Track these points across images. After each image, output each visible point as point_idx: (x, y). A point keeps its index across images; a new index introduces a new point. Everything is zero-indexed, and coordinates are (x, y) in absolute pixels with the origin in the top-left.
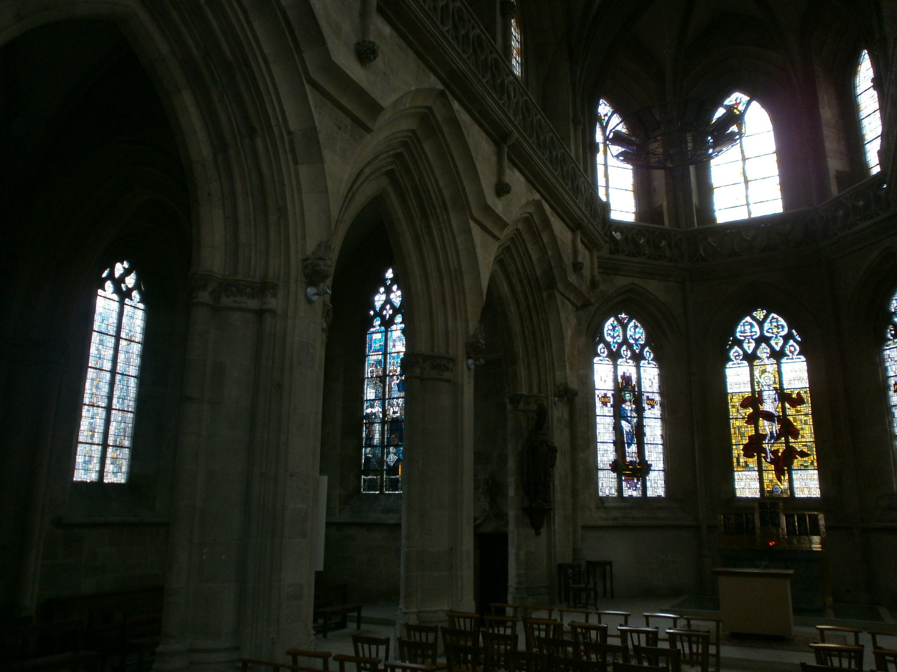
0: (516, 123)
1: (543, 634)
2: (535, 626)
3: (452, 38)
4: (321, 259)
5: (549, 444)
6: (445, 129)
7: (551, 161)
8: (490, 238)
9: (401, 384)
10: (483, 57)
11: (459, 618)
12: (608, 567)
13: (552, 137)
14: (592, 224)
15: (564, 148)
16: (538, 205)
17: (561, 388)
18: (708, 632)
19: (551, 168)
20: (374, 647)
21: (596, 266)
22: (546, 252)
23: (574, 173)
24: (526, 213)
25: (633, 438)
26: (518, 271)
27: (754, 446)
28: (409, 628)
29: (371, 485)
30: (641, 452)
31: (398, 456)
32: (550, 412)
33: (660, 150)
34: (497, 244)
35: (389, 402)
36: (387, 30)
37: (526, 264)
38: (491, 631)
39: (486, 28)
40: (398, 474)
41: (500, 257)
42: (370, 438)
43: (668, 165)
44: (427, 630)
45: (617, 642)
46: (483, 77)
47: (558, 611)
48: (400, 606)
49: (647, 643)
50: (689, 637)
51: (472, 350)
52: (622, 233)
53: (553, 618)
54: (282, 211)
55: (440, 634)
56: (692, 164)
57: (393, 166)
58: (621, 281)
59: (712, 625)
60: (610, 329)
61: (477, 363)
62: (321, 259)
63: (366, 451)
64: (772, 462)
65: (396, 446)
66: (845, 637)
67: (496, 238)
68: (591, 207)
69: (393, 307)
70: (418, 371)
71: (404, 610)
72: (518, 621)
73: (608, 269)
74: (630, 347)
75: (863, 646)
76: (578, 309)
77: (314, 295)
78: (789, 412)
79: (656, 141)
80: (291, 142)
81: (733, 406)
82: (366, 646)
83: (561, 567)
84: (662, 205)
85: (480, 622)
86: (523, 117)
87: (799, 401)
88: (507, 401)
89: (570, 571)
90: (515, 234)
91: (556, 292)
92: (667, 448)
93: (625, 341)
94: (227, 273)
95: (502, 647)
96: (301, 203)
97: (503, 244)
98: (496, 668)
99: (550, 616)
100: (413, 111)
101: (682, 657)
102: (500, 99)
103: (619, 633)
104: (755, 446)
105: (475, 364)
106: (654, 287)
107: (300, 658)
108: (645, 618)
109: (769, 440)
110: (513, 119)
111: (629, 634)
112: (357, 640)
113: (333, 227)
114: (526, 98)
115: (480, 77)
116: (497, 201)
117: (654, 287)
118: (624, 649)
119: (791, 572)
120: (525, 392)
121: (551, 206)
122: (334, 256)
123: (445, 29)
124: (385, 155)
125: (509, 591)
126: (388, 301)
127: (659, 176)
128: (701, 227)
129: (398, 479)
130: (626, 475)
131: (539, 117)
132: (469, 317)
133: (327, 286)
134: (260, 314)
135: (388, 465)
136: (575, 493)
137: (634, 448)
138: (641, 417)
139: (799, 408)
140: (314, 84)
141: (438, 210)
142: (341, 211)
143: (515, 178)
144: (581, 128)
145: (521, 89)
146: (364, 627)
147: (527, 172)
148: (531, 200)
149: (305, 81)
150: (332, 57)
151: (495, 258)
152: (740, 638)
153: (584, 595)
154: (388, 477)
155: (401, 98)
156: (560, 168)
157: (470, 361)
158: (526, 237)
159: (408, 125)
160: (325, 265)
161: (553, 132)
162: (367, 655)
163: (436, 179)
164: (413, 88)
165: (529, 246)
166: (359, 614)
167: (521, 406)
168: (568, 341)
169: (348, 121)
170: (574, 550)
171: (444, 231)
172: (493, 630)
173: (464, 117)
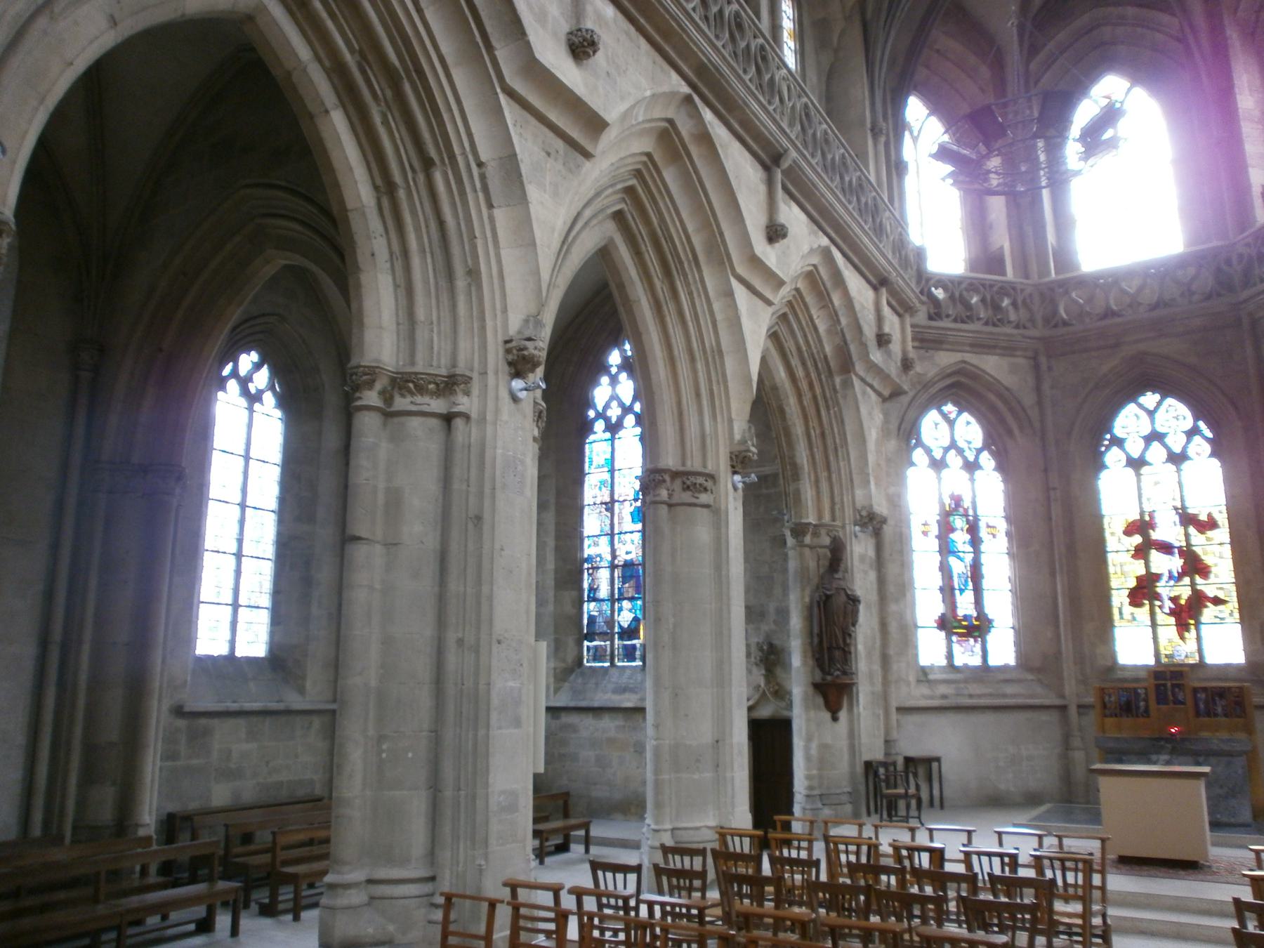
0: (793, 137)
1: (853, 858)
2: (842, 847)
3: (700, 19)
4: (529, 339)
5: (849, 593)
6: (694, 150)
7: (843, 190)
9: (636, 513)
10: (743, 45)
11: (732, 835)
12: (935, 765)
13: (843, 155)
14: (903, 279)
15: (861, 170)
16: (826, 254)
17: (864, 513)
19: (843, 200)
20: (620, 876)
22: (839, 321)
23: (875, 205)
24: (809, 265)
25: (966, 581)
27: (1144, 591)
28: (666, 850)
29: (598, 655)
31: (635, 613)
32: (848, 548)
34: (770, 310)
35: (620, 538)
37: (810, 338)
38: (777, 853)
40: (639, 638)
42: (593, 590)
43: (1018, 189)
44: (692, 853)
48: (647, 821)
50: (1062, 861)
51: (739, 462)
52: (945, 289)
53: (865, 835)
54: (473, 273)
55: (710, 860)
58: (946, 359)
60: (932, 426)
61: (747, 480)
62: (529, 339)
63: (590, 608)
65: (632, 599)
67: (769, 303)
68: (900, 254)
69: (621, 404)
70: (664, 494)
71: (653, 827)
72: (817, 839)
73: (926, 342)
74: (960, 452)
76: (885, 400)
77: (521, 390)
78: (1194, 541)
80: (483, 177)
81: (1113, 534)
82: (609, 875)
83: (868, 765)
84: (1002, 248)
85: (763, 844)
88: (788, 533)
89: (882, 771)
90: (794, 296)
92: (1016, 595)
93: (953, 445)
94: (401, 363)
95: (798, 877)
96: (499, 262)
97: (777, 311)
98: (787, 906)
99: (860, 832)
100: (647, 125)
102: (770, 103)
103: (962, 856)
104: (1145, 591)
105: (744, 483)
106: (992, 365)
107: (520, 890)
110: (788, 131)
112: (596, 866)
113: (544, 294)
114: (805, 99)
115: (741, 72)
116: (768, 248)
117: (992, 365)
119: (1206, 769)
120: (812, 519)
122: (546, 333)
124: (610, 191)
125: (795, 800)
126: (614, 397)
127: (997, 207)
128: (1061, 277)
129: (634, 647)
130: (960, 635)
131: (825, 126)
132: (734, 416)
133: (537, 376)
134: (448, 419)
135: (620, 626)
136: (885, 660)
140: (511, 94)
141: (686, 265)
142: (553, 270)
143: (792, 216)
144: (883, 139)
145: (798, 88)
146: (594, 850)
148: (815, 246)
149: (499, 90)
150: (538, 56)
151: (768, 331)
152: (1131, 863)
153: (902, 804)
154: (621, 642)
155: (633, 107)
156: (855, 199)
157: (737, 478)
158: (810, 299)
159: (645, 144)
160: (536, 348)
161: (844, 147)
162: (611, 887)
164: (648, 93)
165: (814, 312)
166: (587, 832)
167: (808, 539)
168: (871, 445)
169: (559, 144)
170: (887, 742)
171: (695, 295)
172: (781, 853)
173: (719, 132)
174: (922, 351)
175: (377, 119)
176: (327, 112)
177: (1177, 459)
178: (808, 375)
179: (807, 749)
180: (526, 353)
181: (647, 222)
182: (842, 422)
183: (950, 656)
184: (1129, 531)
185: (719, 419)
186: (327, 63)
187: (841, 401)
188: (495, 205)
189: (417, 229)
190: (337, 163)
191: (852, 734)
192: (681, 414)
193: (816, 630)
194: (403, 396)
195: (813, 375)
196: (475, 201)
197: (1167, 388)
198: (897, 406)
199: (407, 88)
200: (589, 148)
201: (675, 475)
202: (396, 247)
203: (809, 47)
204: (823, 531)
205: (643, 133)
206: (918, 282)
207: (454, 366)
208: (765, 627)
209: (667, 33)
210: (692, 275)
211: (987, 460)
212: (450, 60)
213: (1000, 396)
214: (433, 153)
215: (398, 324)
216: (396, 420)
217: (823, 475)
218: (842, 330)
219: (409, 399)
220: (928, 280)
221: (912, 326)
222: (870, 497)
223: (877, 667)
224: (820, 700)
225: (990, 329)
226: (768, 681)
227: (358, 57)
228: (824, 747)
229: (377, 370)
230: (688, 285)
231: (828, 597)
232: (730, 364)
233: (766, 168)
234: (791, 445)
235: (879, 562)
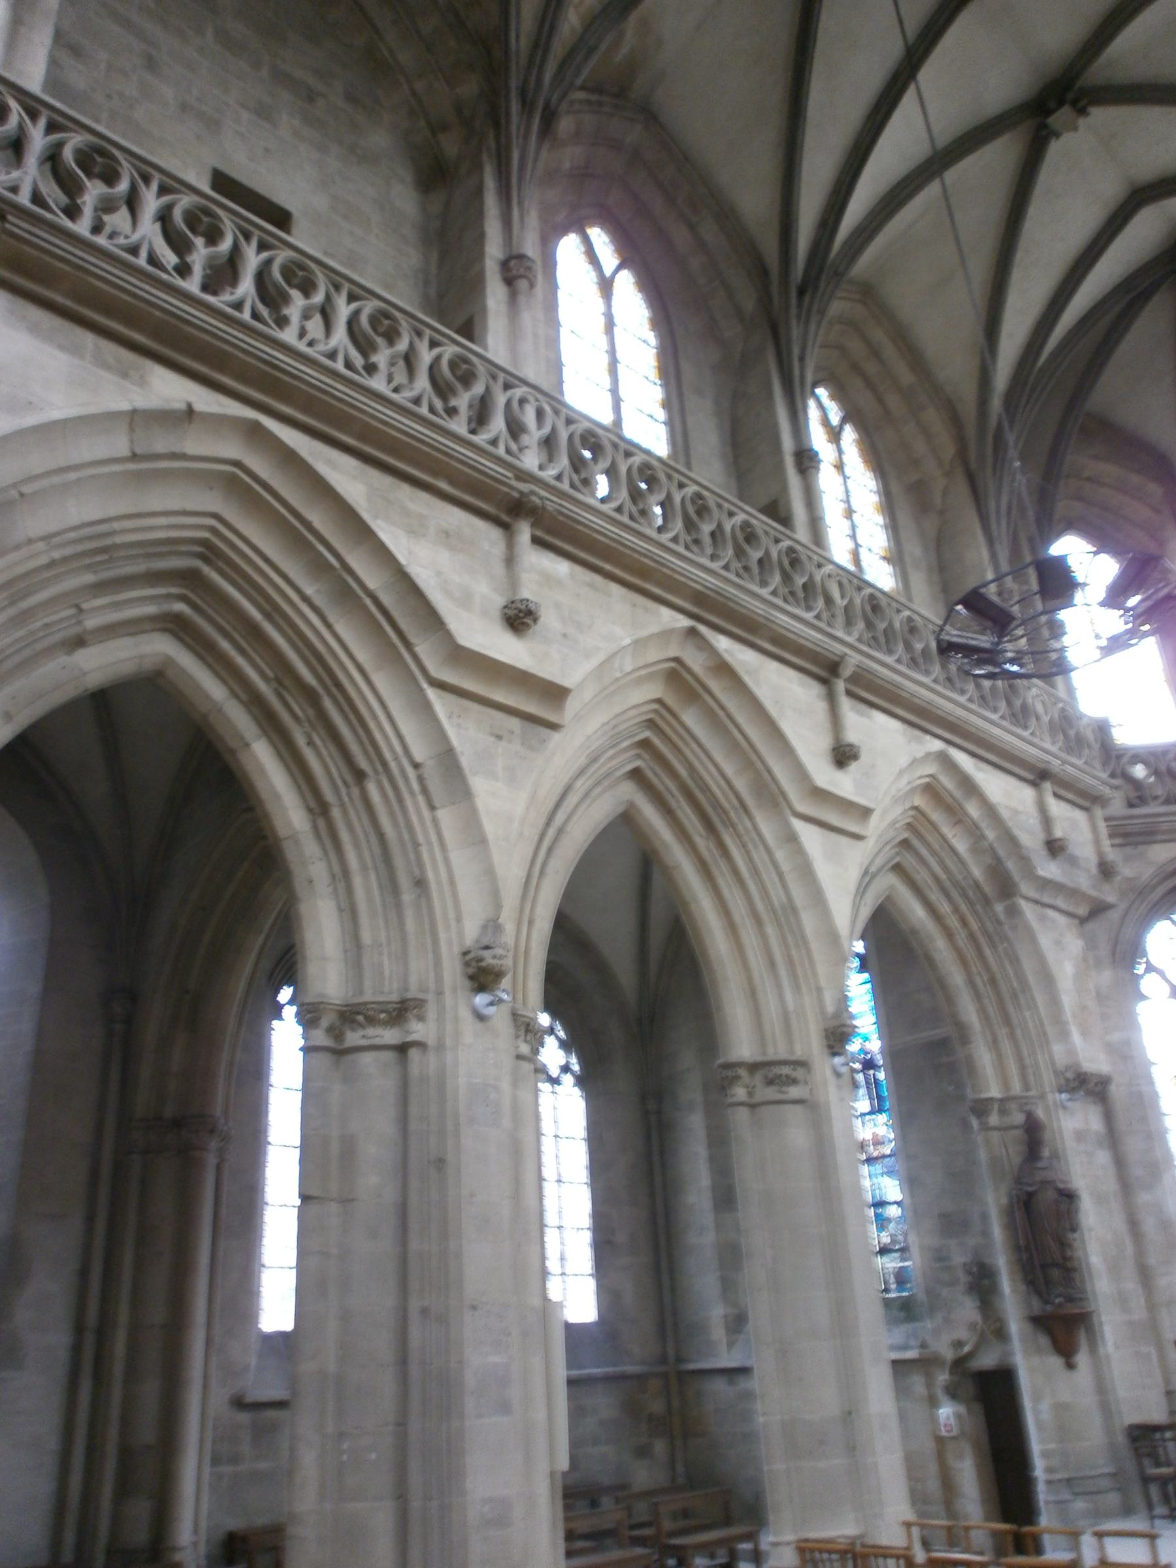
4: (487, 948)
6: (714, 685)
8: (844, 840)
17: (1070, 1075)
22: (982, 837)
26: (936, 878)
52: (1146, 763)
54: (420, 883)
62: (487, 948)
76: (1083, 921)
80: (421, 779)
100: (643, 672)
120: (994, 1092)
124: (612, 752)
132: (823, 983)
141: (732, 814)
158: (936, 816)
159: (655, 690)
160: (494, 957)
163: (716, 766)
164: (627, 641)
167: (994, 1119)
169: (515, 723)
174: (1128, 850)
175: (300, 741)
176: (247, 745)
178: (956, 910)
179: (1037, 1413)
180: (483, 964)
186: (244, 697)
187: (1010, 933)
188: (438, 806)
189: (357, 846)
190: (264, 794)
191: (1102, 1389)
194: (353, 1030)
195: (963, 907)
196: (415, 805)
198: (1100, 928)
199: (328, 704)
200: (552, 717)
201: (754, 1067)
202: (337, 869)
203: (904, 518)
204: (1013, 1106)
205: (650, 677)
206: (1105, 764)
207: (406, 990)
208: (972, 1241)
209: (644, 573)
212: (368, 667)
214: (363, 764)
215: (345, 951)
216: (350, 1057)
217: (1002, 1032)
218: (992, 848)
219: (361, 1033)
220: (1119, 757)
221: (1107, 819)
222: (1072, 1052)
223: (1131, 1285)
224: (1044, 1341)
227: (275, 685)
228: (1060, 1408)
229: (322, 1006)
230: (739, 836)
231: (1030, 1195)
233: (824, 681)
234: (950, 1000)
235: (1112, 1138)
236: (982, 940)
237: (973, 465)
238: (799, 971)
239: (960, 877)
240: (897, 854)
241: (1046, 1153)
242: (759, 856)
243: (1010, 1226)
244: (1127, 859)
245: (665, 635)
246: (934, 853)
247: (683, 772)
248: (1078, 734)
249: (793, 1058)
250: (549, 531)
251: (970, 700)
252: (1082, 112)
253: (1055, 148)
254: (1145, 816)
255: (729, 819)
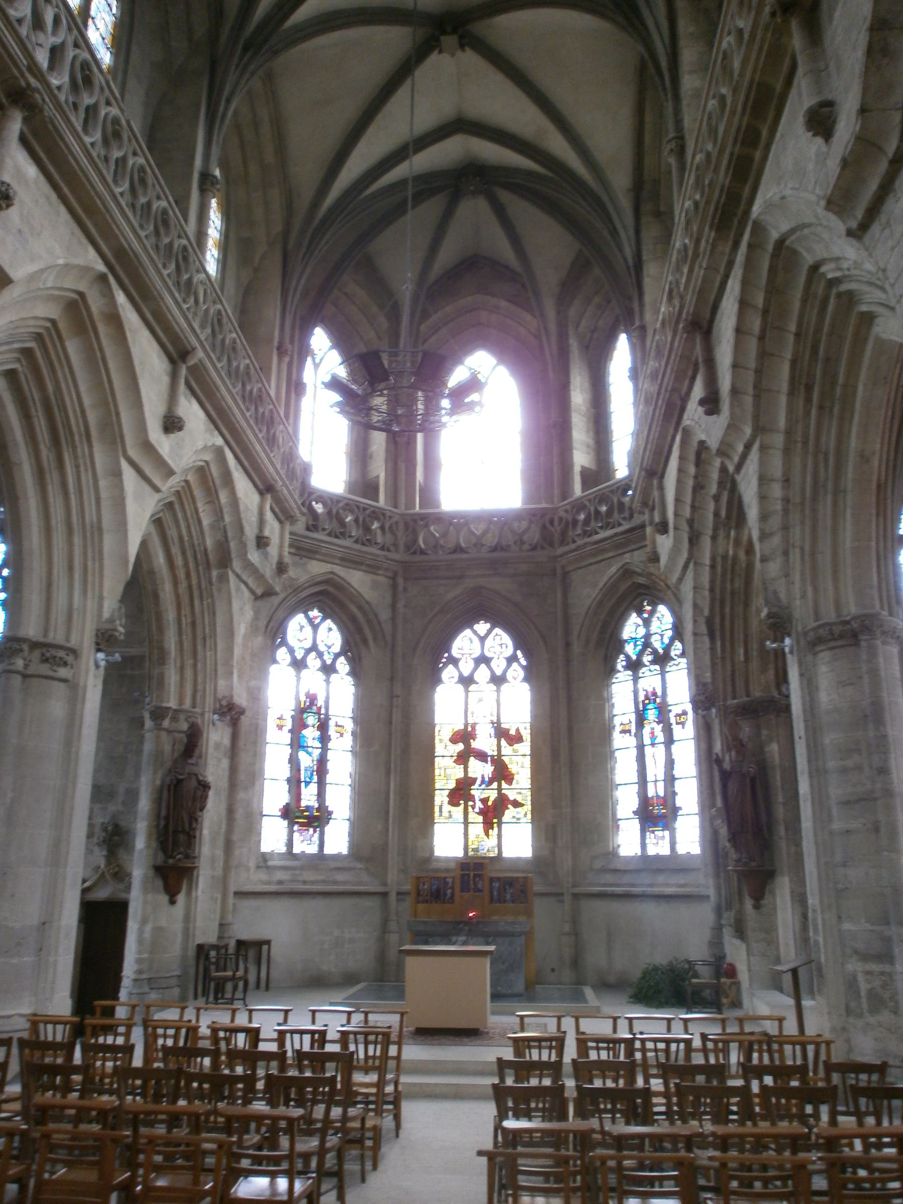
0: (203, 338)
6: (102, 328)
7: (243, 397)
8: (147, 488)
10: (166, 240)
12: (265, 948)
13: (248, 365)
14: (287, 488)
15: (262, 383)
16: (219, 452)
18: (389, 1027)
21: (287, 544)
22: (222, 518)
25: (312, 775)
26: (181, 538)
30: (321, 795)
32: (205, 736)
33: (384, 408)
34: (157, 496)
36: (32, 171)
39: (176, 202)
41: (158, 516)
45: (273, 1047)
46: (165, 266)
47: (195, 1008)
49: (312, 1047)
52: (325, 504)
53: (186, 1018)
55: (15, 1051)
56: (420, 431)
57: (16, 366)
58: (317, 568)
59: (393, 1020)
61: (110, 658)
64: (481, 812)
66: (545, 1025)
67: (157, 490)
68: (288, 465)
74: (320, 655)
75: (565, 1032)
76: (257, 598)
79: (381, 395)
83: (200, 947)
84: (378, 477)
85: (78, 1031)
86: (213, 331)
87: (516, 739)
88: (147, 715)
89: (213, 953)
90: (183, 487)
91: (230, 573)
93: (314, 648)
100: (57, 293)
101: (355, 1063)
102: (185, 301)
106: (356, 579)
108: (310, 1013)
109: (480, 785)
110: (198, 331)
111: (288, 1035)
115: (160, 266)
117: (356, 579)
118: (281, 1056)
119: (492, 948)
120: (172, 704)
121: (237, 457)
123: (118, 190)
127: (379, 440)
128: (423, 511)
130: (301, 824)
131: (234, 335)
132: (105, 594)
136: (229, 846)
137: (313, 788)
138: (325, 749)
139: (516, 746)
141: (77, 438)
144: (287, 359)
147: (209, 408)
148: (210, 444)
151: (152, 516)
152: (426, 1034)
153: (229, 986)
155: (42, 271)
157: (101, 656)
158: (198, 493)
159: (52, 311)
164: (61, 261)
167: (166, 723)
168: (239, 639)
170: (221, 925)
171: (82, 469)
173: (130, 316)
174: (297, 558)
177: (498, 680)
178: (186, 564)
181: (42, 387)
182: (214, 614)
183: (290, 844)
184: (454, 740)
185: (90, 594)
187: (215, 593)
191: (188, 918)
192: (49, 585)
193: (164, 813)
195: (192, 565)
197: (497, 620)
201: (35, 645)
203: (231, 262)
204: (182, 717)
205: (56, 298)
208: (112, 808)
210: (82, 449)
211: (343, 665)
213: (360, 608)
217: (189, 662)
218: (225, 527)
220: (310, 494)
221: (291, 533)
222: (231, 688)
223: (220, 853)
224: (159, 883)
225: (357, 547)
226: (109, 863)
230: (76, 457)
231: (179, 782)
232: (109, 542)
233: (172, 361)
234: (161, 630)
235: (234, 751)
236: (196, 593)
237: (290, 246)
238: (90, 579)
239: (196, 542)
240: (162, 510)
241: (197, 753)
242: (86, 479)
243: (158, 801)
244: (295, 564)
245: (86, 269)
246: (186, 519)
247: (50, 388)
248: (293, 468)
249: (69, 645)
250: (35, 134)
251: (250, 416)
252: (462, 46)
253: (434, 58)
254: (314, 539)
255: (73, 441)
